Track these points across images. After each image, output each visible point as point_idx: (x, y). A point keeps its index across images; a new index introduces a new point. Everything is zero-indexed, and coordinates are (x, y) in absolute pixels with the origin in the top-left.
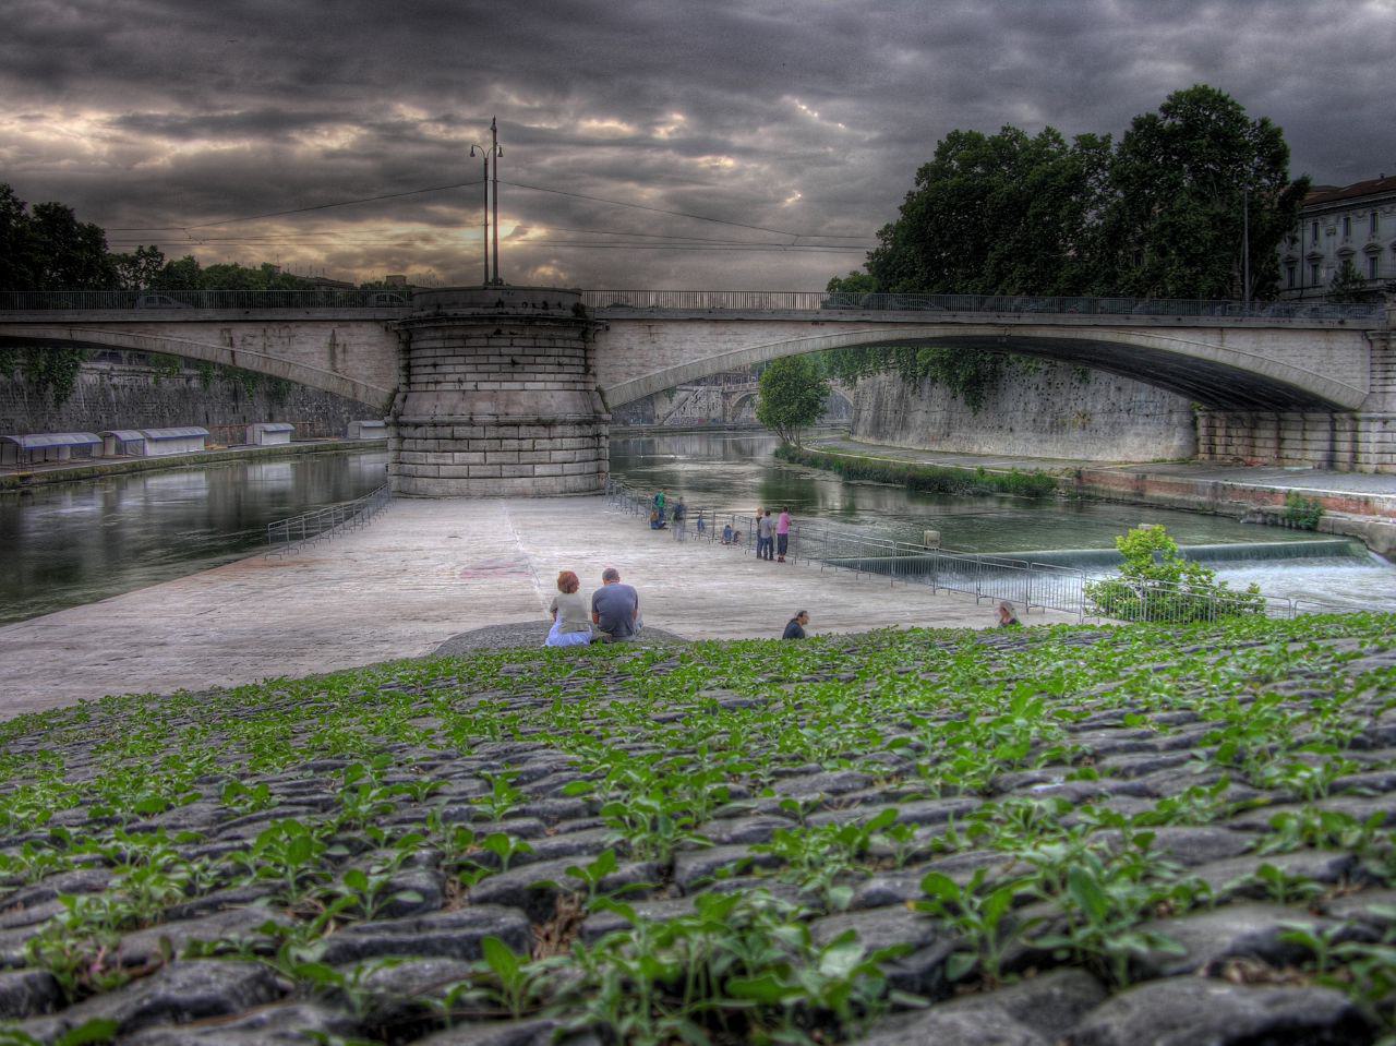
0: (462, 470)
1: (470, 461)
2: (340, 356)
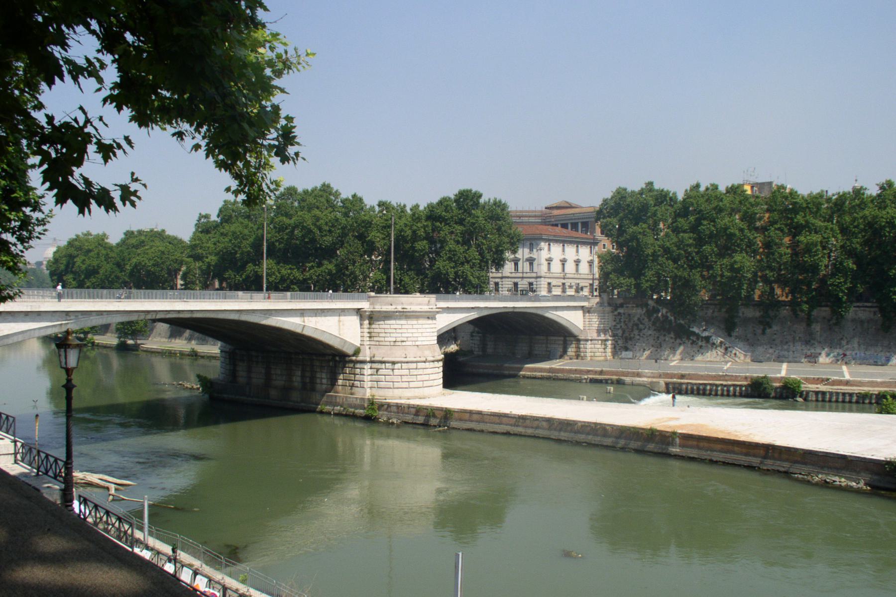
2: (341, 327)
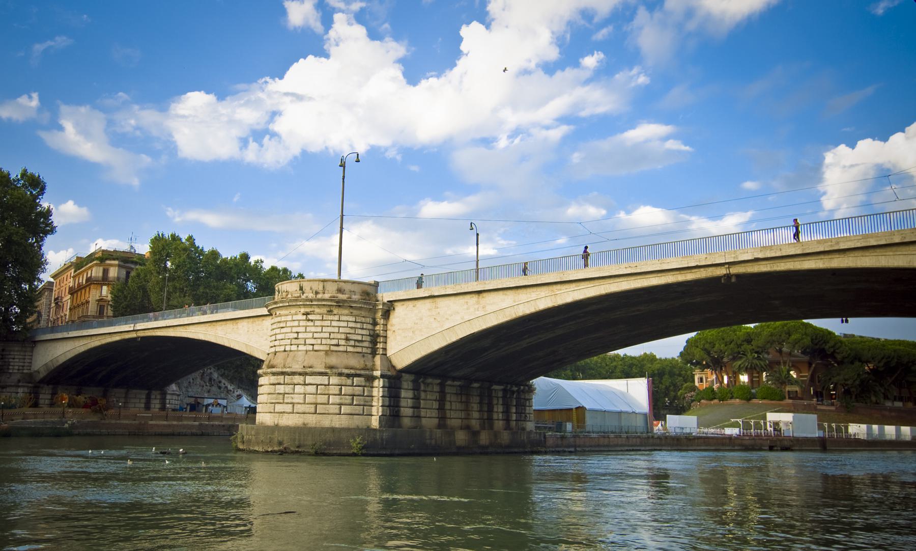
0: (309, 379)
1: (296, 382)
